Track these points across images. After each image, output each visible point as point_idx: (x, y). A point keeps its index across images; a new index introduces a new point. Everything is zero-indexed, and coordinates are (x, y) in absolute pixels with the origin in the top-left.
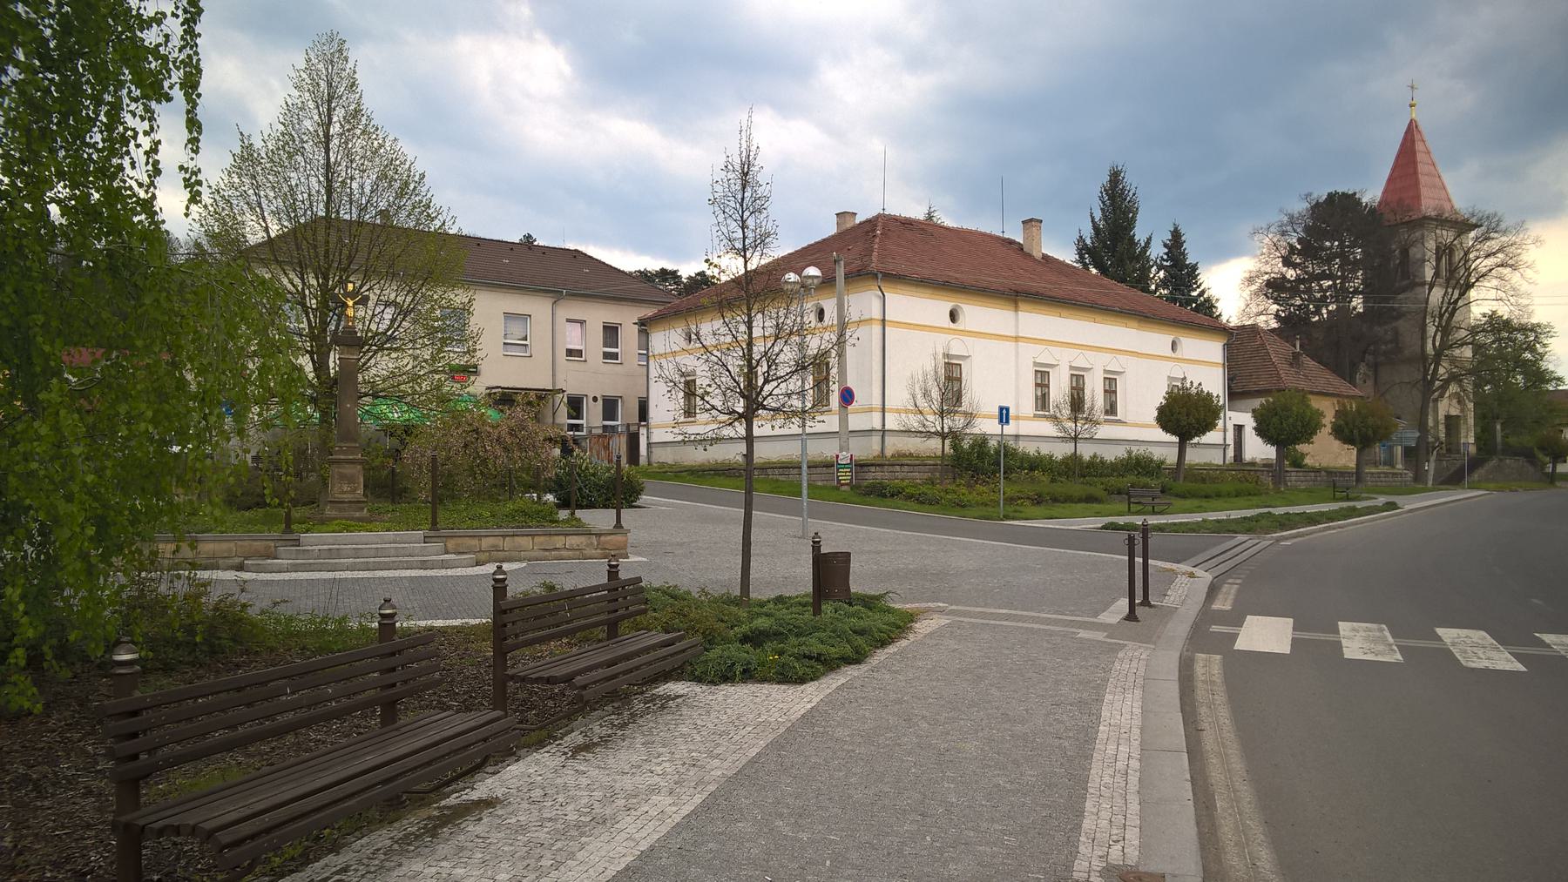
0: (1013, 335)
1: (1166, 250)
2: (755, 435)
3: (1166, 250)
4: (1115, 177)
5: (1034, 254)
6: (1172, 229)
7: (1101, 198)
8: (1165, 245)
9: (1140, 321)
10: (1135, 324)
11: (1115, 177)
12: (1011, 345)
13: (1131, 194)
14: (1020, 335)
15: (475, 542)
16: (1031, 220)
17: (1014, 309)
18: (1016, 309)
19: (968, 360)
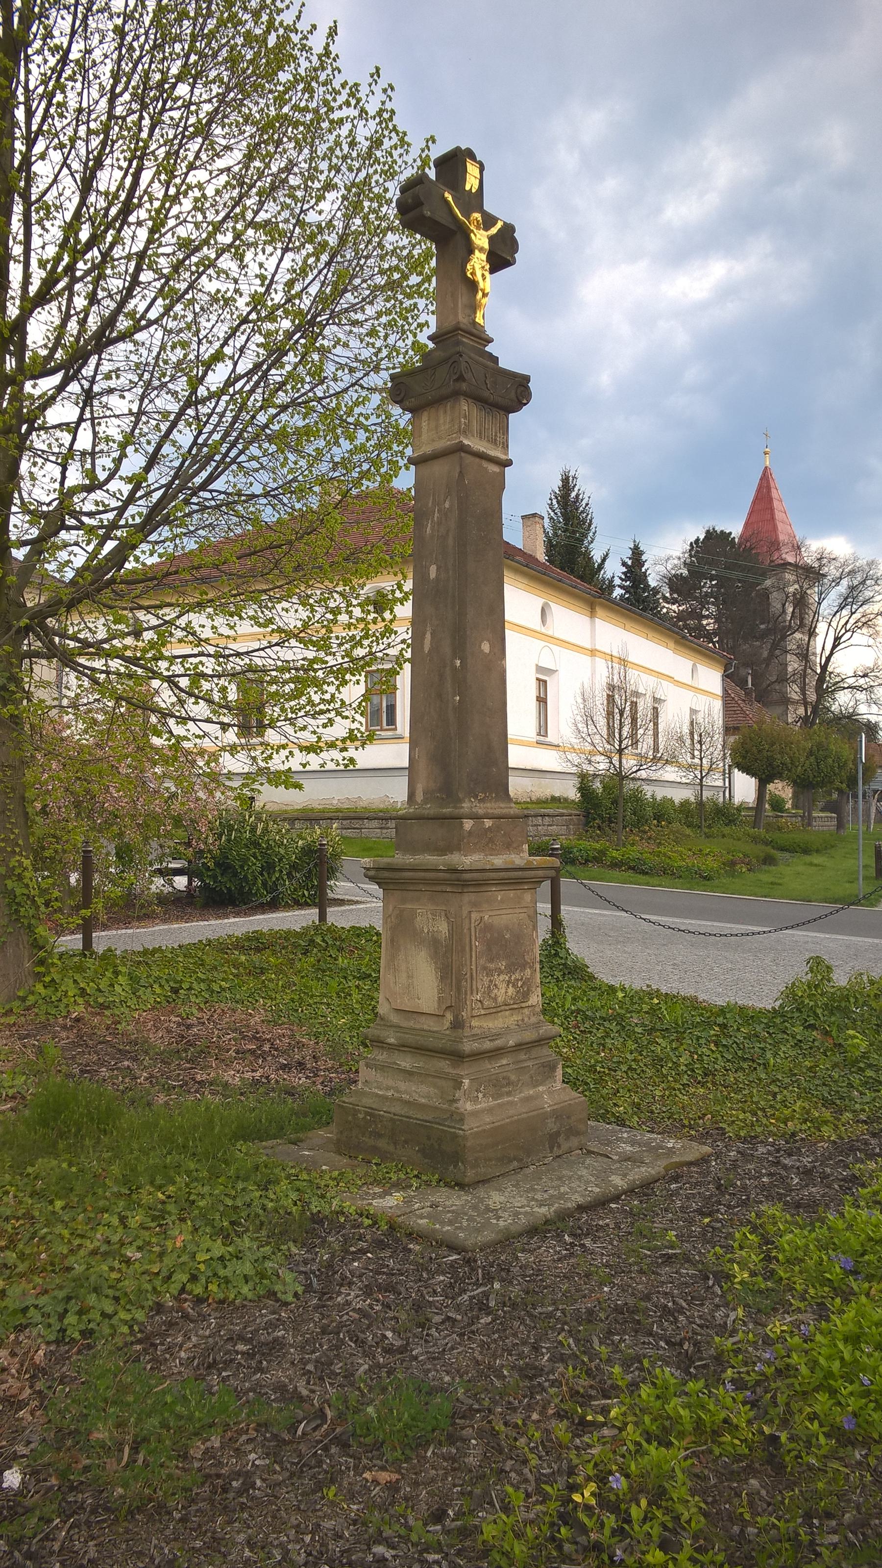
0: (589, 646)
1: (624, 569)
2: (511, 764)
3: (624, 569)
4: (567, 484)
5: (44, 662)
6: (632, 546)
7: (551, 506)
8: (624, 564)
9: (677, 642)
10: (672, 644)
11: (567, 484)
12: (586, 660)
13: (584, 503)
14: (598, 647)
15: (411, 1113)
16: (534, 515)
17: (589, 614)
18: (592, 615)
19: (555, 676)
